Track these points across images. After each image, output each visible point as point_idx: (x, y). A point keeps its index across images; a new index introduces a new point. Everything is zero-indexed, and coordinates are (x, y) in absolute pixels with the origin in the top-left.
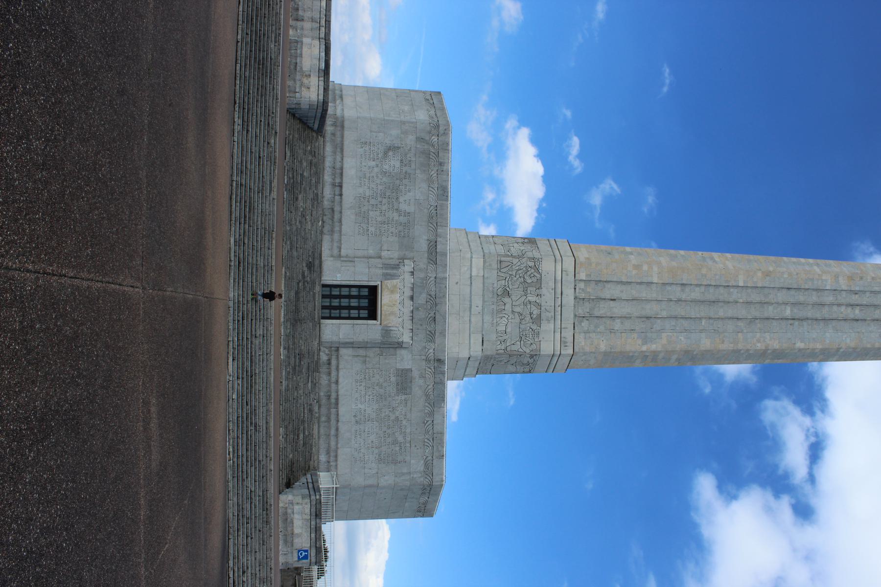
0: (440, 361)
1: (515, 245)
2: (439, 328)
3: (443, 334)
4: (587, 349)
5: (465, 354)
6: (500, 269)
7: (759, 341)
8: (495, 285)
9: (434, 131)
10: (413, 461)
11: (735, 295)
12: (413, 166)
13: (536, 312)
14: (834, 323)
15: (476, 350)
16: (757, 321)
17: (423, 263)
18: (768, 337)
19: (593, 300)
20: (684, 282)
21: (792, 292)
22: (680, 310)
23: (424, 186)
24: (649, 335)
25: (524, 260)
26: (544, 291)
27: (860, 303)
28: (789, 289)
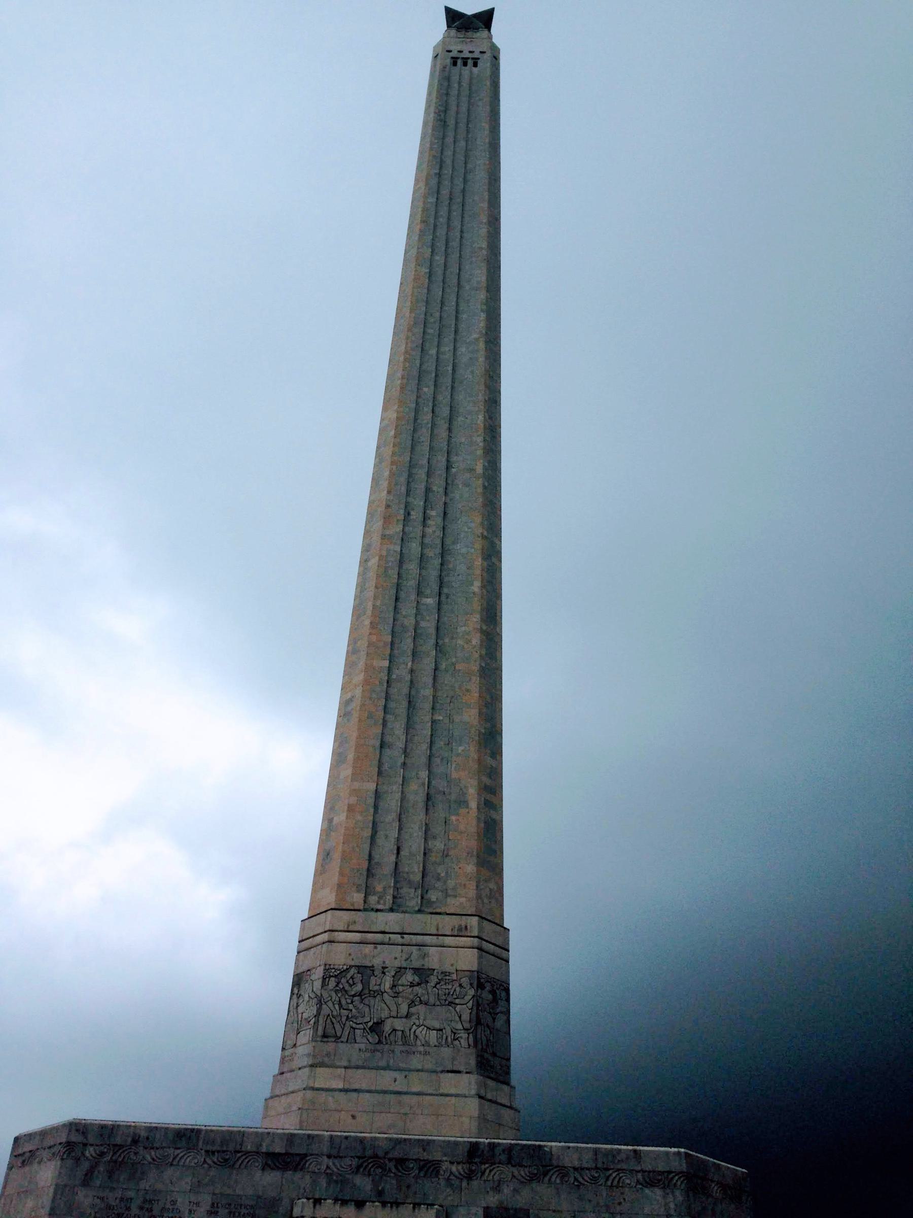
0: (474, 1150)
1: (300, 1010)
2: (415, 1153)
3: (425, 1145)
4: (472, 893)
5: (472, 1106)
6: (337, 1038)
7: (468, 642)
8: (363, 1046)
9: (78, 1152)
10: (646, 1210)
11: (402, 671)
12: (131, 1194)
13: (409, 977)
14: (448, 541)
15: (468, 1083)
16: (440, 642)
17: (303, 1180)
18: (463, 629)
19: (396, 882)
20: (378, 744)
21: (402, 595)
22: (421, 749)
23: (169, 1172)
24: (453, 797)
25: (325, 995)
26: (377, 962)
27: (422, 510)
28: (397, 599)
